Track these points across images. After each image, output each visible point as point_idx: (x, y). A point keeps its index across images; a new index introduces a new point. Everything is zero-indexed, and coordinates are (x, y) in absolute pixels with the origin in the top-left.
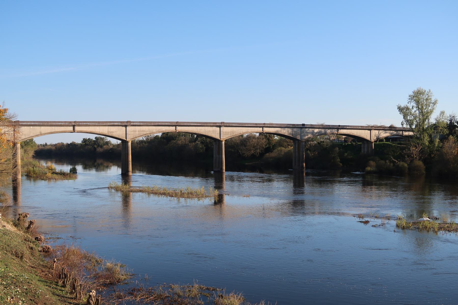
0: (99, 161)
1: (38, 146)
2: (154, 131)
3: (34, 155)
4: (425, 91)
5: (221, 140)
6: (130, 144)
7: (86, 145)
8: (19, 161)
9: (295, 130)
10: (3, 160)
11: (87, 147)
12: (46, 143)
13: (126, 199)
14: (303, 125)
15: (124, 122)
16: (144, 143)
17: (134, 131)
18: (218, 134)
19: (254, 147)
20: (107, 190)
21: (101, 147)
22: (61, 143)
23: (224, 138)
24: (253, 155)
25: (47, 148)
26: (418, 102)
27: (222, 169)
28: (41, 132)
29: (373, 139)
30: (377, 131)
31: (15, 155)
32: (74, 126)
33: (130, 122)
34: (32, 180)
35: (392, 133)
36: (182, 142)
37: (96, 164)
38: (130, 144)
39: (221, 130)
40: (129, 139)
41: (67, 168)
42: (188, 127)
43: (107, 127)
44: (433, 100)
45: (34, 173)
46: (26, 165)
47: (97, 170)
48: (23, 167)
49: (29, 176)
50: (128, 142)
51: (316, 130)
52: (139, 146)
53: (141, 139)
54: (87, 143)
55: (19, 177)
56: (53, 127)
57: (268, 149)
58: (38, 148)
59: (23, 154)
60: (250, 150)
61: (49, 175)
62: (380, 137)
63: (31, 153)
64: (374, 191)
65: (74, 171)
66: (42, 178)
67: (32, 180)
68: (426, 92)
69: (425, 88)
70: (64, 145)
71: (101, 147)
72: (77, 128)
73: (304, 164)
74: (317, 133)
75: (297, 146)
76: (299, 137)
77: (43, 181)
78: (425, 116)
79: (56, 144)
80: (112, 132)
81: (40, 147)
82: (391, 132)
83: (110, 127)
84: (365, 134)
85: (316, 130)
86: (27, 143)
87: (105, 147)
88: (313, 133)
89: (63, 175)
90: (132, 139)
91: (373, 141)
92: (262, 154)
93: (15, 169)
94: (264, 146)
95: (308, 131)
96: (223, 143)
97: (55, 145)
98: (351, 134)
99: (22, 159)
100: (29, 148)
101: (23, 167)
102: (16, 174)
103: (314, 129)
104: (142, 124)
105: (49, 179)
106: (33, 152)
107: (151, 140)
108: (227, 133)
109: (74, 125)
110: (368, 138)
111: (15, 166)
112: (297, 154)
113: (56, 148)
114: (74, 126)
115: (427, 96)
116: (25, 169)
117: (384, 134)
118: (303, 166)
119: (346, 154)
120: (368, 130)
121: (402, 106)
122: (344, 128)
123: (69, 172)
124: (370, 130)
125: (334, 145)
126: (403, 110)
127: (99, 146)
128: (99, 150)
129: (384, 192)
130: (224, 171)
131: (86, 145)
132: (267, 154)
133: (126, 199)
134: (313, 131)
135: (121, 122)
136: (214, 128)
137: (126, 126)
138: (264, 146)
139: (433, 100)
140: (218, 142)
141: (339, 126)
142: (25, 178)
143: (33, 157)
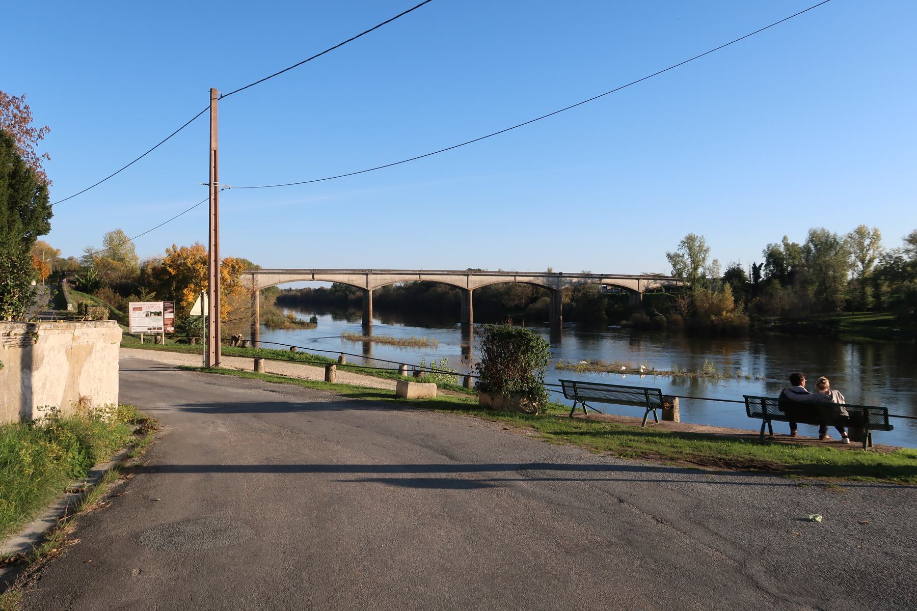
0: (351, 310)
1: (282, 291)
2: (397, 279)
3: (276, 302)
4: (697, 237)
5: (469, 289)
6: (371, 293)
7: (336, 290)
8: (258, 310)
9: (551, 279)
10: (242, 309)
11: (338, 293)
12: (290, 288)
13: (366, 349)
14: (561, 274)
15: (365, 270)
16: (401, 290)
17: (375, 280)
18: (465, 283)
19: (518, 296)
20: (339, 340)
21: (354, 293)
22: (309, 288)
23: (471, 287)
24: (517, 305)
25: (293, 293)
26: (690, 248)
27: (469, 320)
28: (279, 281)
29: (642, 289)
30: (646, 281)
31: (253, 304)
32: (313, 274)
33: (371, 270)
34: (271, 329)
35: (663, 283)
36: (442, 289)
37: (347, 313)
38: (371, 293)
39: (469, 279)
40: (371, 289)
41: (306, 318)
42: (432, 276)
43: (347, 275)
44: (705, 248)
45: (273, 323)
46: (267, 313)
47: (349, 320)
48: (261, 315)
49: (267, 325)
50: (368, 291)
51: (575, 280)
52: (396, 293)
53: (398, 284)
54: (338, 288)
55: (258, 325)
56: (292, 275)
57: (534, 300)
58: (281, 294)
59: (263, 300)
60: (515, 300)
61: (287, 324)
62: (650, 287)
63: (273, 300)
64: (643, 345)
65: (314, 321)
66: (280, 327)
67: (271, 329)
68: (699, 238)
69: (697, 233)
70: (311, 291)
71: (354, 293)
72: (316, 276)
73: (561, 317)
74: (576, 282)
75: (554, 297)
76: (554, 287)
77: (282, 330)
78: (696, 264)
79: (302, 289)
80: (353, 280)
81: (284, 293)
82: (663, 282)
83: (350, 275)
84: (632, 284)
85: (575, 280)
86: (266, 291)
87: (358, 293)
88: (571, 283)
89: (302, 324)
90: (373, 288)
91: (641, 292)
92: (527, 305)
93: (253, 317)
94: (530, 295)
95: (565, 281)
96: (471, 292)
97: (301, 290)
98: (616, 284)
99: (261, 307)
100: (270, 294)
101: (263, 316)
102: (253, 325)
103: (571, 278)
104: (383, 272)
105: (288, 328)
106: (275, 298)
107: (409, 286)
108: (475, 282)
109: (313, 273)
110: (636, 289)
111: (254, 314)
112: (554, 304)
113: (302, 294)
114: (313, 274)
115: (699, 242)
116: (264, 318)
117: (654, 285)
118: (560, 319)
119: (616, 306)
120: (636, 279)
121: (672, 253)
122: (607, 276)
123: (309, 321)
124: (638, 279)
125: (601, 296)
126: (672, 258)
127: (351, 292)
128: (351, 296)
129: (444, 330)
130: (472, 323)
131: (336, 290)
132: (531, 305)
133: (366, 349)
134: (571, 280)
135: (363, 270)
136: (461, 277)
137: (367, 274)
138: (530, 295)
139: (705, 248)
140: (465, 291)
141: (602, 275)
142: (263, 327)
143: (275, 304)
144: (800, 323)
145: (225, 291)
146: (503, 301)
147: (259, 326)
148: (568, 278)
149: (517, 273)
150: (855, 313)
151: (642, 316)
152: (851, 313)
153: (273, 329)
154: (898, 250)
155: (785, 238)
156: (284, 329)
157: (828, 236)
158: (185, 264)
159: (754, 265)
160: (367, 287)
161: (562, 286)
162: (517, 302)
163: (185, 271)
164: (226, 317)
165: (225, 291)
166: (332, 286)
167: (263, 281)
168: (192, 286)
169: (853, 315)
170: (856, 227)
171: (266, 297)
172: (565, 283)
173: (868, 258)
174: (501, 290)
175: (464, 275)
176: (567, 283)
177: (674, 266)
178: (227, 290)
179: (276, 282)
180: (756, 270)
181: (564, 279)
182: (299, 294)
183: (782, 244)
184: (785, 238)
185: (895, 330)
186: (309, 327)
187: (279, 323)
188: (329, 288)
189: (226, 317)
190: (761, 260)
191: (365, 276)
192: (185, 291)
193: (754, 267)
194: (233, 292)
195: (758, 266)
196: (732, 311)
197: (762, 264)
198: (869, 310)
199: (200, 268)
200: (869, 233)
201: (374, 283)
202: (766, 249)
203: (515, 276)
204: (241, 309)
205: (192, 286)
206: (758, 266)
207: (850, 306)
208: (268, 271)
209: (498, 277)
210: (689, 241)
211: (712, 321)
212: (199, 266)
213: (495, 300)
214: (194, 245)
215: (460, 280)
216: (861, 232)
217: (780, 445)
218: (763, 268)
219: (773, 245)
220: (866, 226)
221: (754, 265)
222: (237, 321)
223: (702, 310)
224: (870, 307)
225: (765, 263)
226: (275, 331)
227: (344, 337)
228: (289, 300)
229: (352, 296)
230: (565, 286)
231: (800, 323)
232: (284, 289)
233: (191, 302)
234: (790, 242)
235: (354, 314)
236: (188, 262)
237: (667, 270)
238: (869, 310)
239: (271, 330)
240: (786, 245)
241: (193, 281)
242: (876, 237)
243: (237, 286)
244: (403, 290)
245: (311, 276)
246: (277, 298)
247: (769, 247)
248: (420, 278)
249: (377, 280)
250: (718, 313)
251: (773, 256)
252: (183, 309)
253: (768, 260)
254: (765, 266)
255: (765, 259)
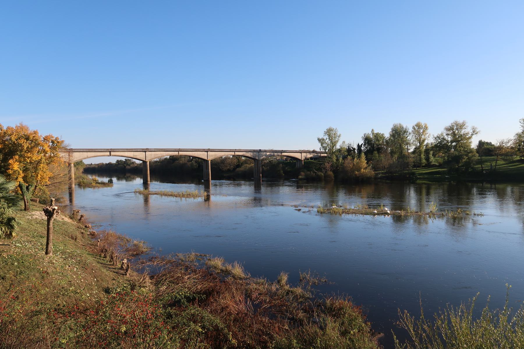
0: (128, 175)
1: (86, 165)
3: (83, 171)
4: (334, 129)
6: (148, 163)
7: (119, 164)
9: (255, 153)
10: (61, 175)
11: (119, 166)
14: (260, 150)
23: (210, 159)
24: (228, 169)
26: (329, 136)
27: (209, 178)
28: (87, 156)
29: (303, 158)
30: (305, 154)
31: (70, 171)
32: (110, 152)
33: (148, 149)
34: (82, 187)
37: (126, 176)
38: (148, 163)
40: (148, 160)
41: (106, 180)
43: (133, 152)
46: (78, 178)
48: (75, 179)
51: (268, 154)
52: (154, 164)
53: (155, 160)
54: (120, 163)
55: (73, 186)
57: (238, 166)
59: (75, 170)
61: (94, 184)
62: (307, 157)
63: (81, 170)
65: (111, 182)
67: (82, 187)
68: (334, 130)
69: (334, 127)
71: (129, 165)
72: (112, 153)
74: (268, 155)
76: (257, 158)
78: (334, 144)
80: (136, 156)
81: (88, 166)
82: (314, 154)
83: (135, 152)
84: (298, 156)
85: (268, 154)
86: (78, 164)
87: (131, 165)
88: (266, 155)
89: (103, 184)
90: (150, 160)
91: (303, 160)
93: (70, 181)
96: (210, 162)
99: (75, 174)
100: (80, 167)
102: (71, 184)
103: (266, 153)
104: (156, 150)
105: (94, 187)
106: (82, 169)
107: (162, 160)
108: (212, 156)
109: (110, 151)
110: (300, 158)
111: (70, 179)
113: (98, 166)
114: (110, 152)
117: (309, 156)
118: (260, 176)
119: (287, 168)
122: (285, 152)
123: (107, 182)
124: (301, 153)
125: (279, 163)
127: (127, 165)
128: (128, 167)
130: (210, 180)
131: (119, 164)
132: (238, 169)
134: (266, 154)
137: (145, 152)
138: (236, 164)
140: (206, 161)
141: (282, 150)
142: (77, 186)
143: (83, 172)
144: (395, 174)
145: (47, 161)
146: (220, 167)
147: (74, 186)
148: (264, 153)
149: (236, 150)
150: (417, 168)
151: (311, 173)
152: (416, 168)
153: (84, 188)
154: (442, 134)
155: (373, 130)
156: (92, 187)
157: (403, 128)
158: (10, 139)
159: (358, 144)
160: (146, 160)
161: (261, 157)
162: (228, 167)
163: (10, 145)
164: (47, 181)
165: (47, 161)
166: (116, 162)
167: (76, 157)
168: (17, 157)
169: (417, 169)
170: (415, 123)
171: (77, 168)
172: (263, 155)
173: (422, 139)
174: (219, 161)
175: (205, 151)
176: (264, 155)
177: (322, 144)
178: (48, 161)
179: (85, 157)
180: (359, 147)
181: (262, 153)
182: (97, 166)
183: (371, 133)
184: (373, 130)
185: (435, 176)
186: (109, 185)
187: (88, 184)
188: (114, 163)
189: (47, 181)
190: (361, 142)
191: (144, 153)
192: (11, 161)
193: (358, 145)
194: (53, 162)
195: (360, 145)
196: (366, 168)
197: (362, 144)
198: (423, 166)
199: (23, 143)
200: (422, 126)
201: (152, 157)
202: (363, 136)
203: (235, 152)
204: (60, 174)
205: (17, 157)
206: (360, 145)
207: (418, 165)
208: (80, 150)
209: (224, 152)
210: (329, 132)
211: (356, 175)
212: (22, 141)
213: (216, 167)
214: (18, 125)
215: (203, 154)
216: (418, 126)
217: (101, 184)
218: (363, 146)
219: (367, 134)
220: (421, 122)
221: (358, 144)
222: (58, 184)
223: (349, 169)
224: (424, 165)
225: (364, 143)
226: (85, 189)
227: (137, 192)
228: (90, 170)
229: (128, 166)
230: (263, 157)
231: (395, 174)
232: (88, 164)
233: (17, 170)
234: (375, 132)
235: (130, 177)
236: (13, 138)
237: (318, 147)
238: (423, 166)
239: (82, 189)
240: (373, 134)
241: (18, 154)
242: (426, 128)
243: (56, 157)
244: (158, 162)
245: (109, 153)
246: (84, 169)
247: (365, 135)
248: (178, 154)
249: (152, 155)
250: (359, 169)
251: (367, 140)
252: (10, 176)
253: (365, 143)
254: (364, 145)
255: (363, 141)
